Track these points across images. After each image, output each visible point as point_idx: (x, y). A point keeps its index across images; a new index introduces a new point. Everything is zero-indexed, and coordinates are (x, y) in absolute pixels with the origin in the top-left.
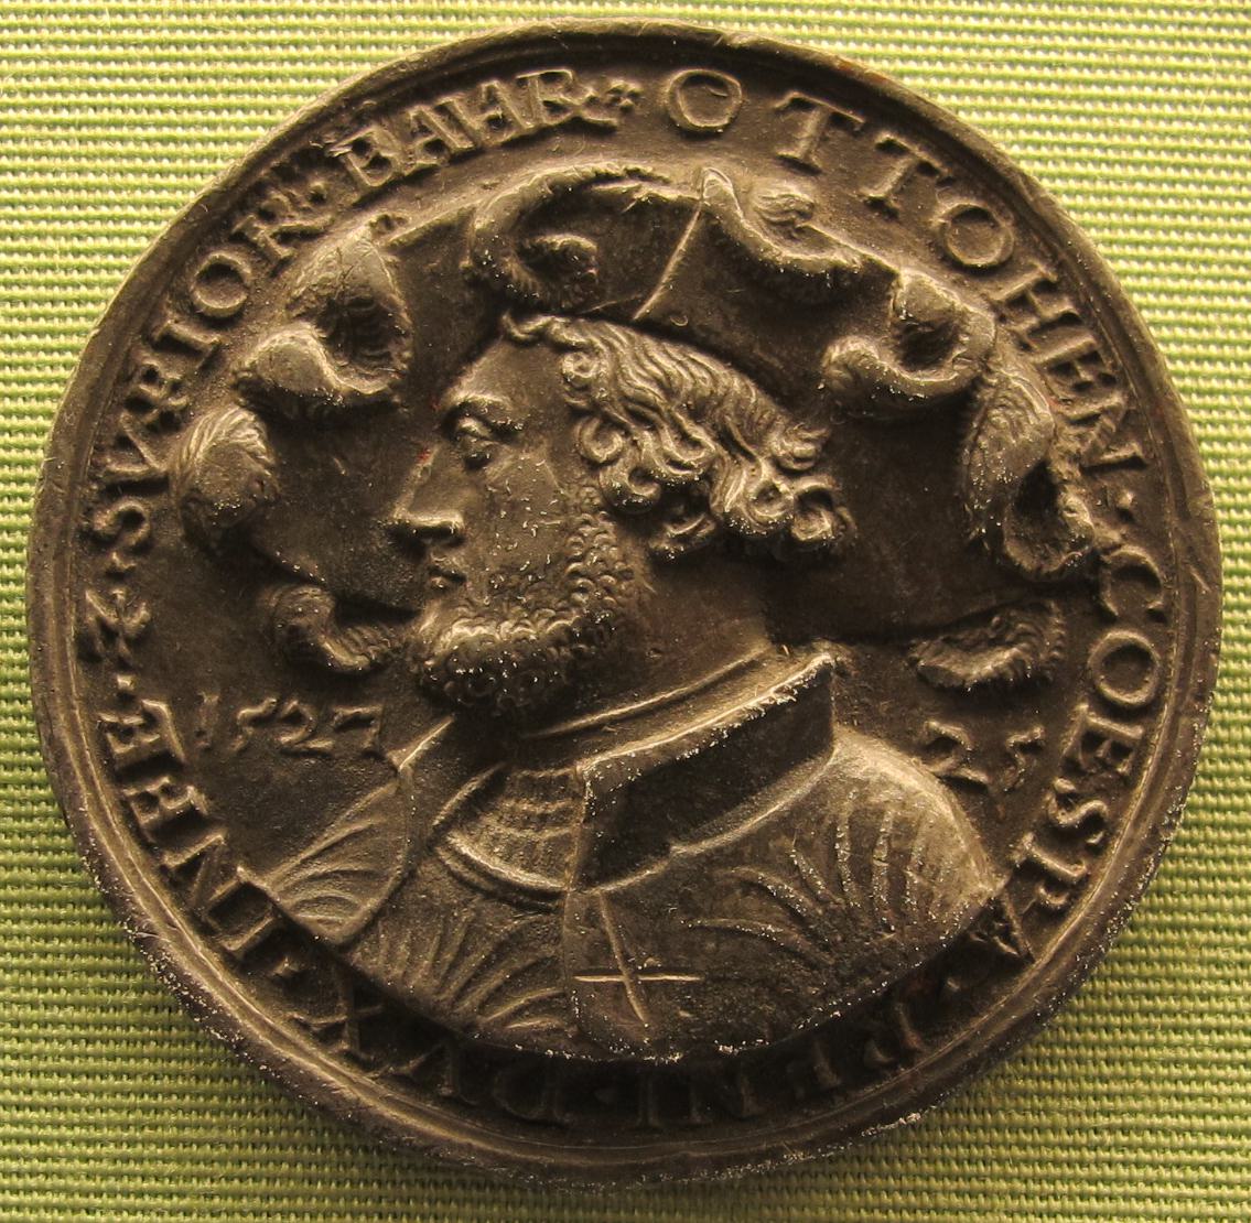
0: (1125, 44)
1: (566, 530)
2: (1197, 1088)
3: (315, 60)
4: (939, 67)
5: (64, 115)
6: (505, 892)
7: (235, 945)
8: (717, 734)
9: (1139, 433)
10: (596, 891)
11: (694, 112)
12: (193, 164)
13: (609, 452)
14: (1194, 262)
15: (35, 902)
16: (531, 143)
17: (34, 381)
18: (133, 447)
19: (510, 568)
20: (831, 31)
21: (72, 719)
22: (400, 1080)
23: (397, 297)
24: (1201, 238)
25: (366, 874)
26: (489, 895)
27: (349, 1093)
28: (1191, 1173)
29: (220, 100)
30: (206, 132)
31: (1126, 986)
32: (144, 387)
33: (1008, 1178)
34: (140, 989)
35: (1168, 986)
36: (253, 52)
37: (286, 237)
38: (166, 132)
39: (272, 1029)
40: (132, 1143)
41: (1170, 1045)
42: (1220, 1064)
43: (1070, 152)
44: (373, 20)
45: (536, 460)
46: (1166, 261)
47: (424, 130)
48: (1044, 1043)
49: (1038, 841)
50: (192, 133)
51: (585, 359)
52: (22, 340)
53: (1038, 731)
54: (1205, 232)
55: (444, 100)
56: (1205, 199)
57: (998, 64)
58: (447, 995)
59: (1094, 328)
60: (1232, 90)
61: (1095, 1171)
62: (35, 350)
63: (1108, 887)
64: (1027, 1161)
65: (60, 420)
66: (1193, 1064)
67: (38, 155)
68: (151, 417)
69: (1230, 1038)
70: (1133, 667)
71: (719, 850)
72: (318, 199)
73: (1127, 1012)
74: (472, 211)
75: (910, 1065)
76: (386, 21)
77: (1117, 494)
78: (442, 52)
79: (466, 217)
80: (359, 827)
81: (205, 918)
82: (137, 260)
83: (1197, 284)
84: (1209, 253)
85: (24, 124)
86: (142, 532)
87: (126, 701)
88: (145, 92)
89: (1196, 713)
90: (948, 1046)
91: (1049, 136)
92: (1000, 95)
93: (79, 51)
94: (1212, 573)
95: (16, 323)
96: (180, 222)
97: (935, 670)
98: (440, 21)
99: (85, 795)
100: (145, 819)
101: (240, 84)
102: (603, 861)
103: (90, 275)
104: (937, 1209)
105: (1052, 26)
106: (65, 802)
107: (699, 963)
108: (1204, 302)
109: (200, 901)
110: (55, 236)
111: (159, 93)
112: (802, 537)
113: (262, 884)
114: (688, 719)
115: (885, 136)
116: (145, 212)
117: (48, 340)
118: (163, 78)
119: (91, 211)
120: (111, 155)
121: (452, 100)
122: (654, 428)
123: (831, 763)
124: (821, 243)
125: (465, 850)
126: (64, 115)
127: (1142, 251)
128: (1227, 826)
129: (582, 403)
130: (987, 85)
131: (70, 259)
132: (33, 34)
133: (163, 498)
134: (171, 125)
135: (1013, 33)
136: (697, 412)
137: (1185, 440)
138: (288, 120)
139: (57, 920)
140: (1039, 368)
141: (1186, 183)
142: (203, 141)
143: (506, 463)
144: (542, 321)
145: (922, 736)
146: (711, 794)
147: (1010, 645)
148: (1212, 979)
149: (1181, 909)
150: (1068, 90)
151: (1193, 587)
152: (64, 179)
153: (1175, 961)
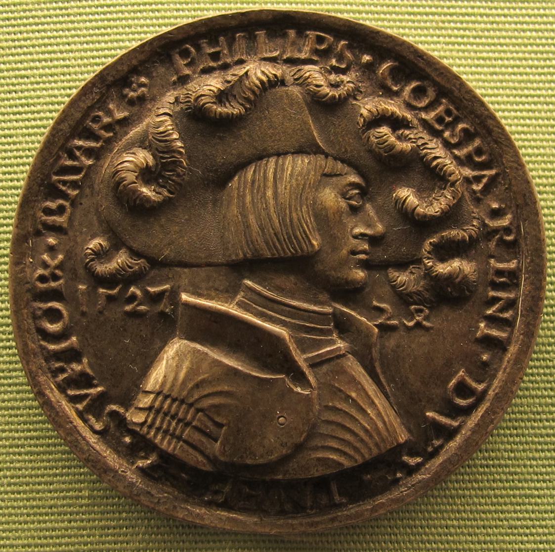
48: (459, 474)
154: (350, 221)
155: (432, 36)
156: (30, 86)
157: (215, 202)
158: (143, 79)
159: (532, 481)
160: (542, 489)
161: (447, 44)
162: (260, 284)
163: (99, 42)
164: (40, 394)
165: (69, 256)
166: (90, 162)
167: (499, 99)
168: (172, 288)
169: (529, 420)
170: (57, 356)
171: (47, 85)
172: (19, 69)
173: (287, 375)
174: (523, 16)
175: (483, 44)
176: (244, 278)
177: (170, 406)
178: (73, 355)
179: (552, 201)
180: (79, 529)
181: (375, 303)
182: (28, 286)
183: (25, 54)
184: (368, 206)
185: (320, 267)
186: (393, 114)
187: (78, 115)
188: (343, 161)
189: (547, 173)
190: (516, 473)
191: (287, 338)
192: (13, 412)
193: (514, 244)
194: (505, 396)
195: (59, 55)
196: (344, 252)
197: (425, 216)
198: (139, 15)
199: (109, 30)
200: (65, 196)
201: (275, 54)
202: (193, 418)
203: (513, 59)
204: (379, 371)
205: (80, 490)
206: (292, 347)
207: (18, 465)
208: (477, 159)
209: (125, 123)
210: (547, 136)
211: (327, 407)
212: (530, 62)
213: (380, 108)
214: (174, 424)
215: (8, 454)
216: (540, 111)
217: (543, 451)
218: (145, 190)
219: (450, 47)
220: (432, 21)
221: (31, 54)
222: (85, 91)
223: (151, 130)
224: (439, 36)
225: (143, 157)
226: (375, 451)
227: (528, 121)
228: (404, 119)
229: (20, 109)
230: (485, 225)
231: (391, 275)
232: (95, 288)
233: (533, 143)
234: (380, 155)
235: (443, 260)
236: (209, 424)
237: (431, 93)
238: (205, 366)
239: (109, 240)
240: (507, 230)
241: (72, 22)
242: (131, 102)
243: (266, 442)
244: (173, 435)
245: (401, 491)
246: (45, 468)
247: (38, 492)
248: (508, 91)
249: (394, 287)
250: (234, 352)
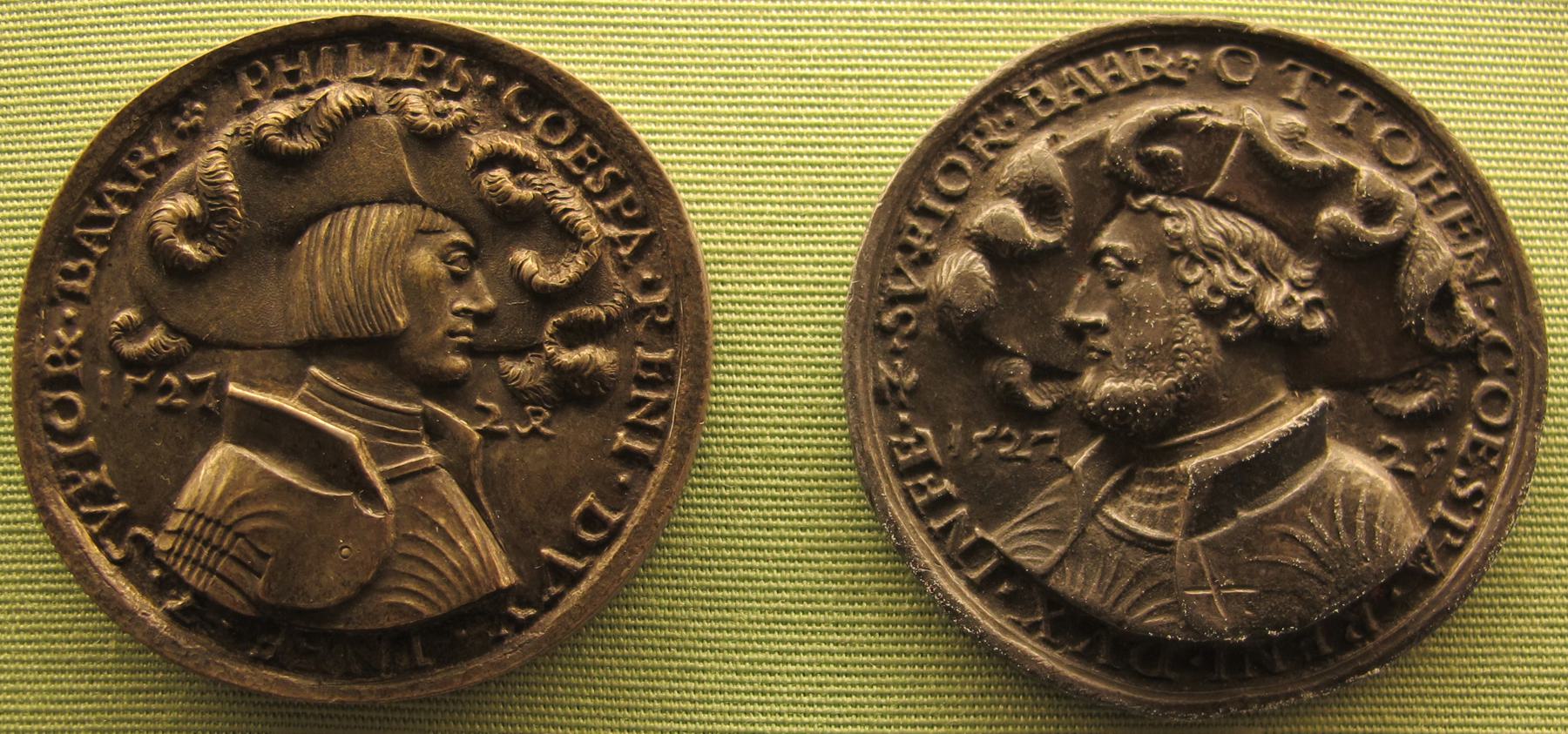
0: (1476, 31)
1: (1172, 324)
2: (1533, 650)
4: (1369, 45)
5: (849, 72)
6: (1139, 541)
7: (975, 575)
8: (1266, 446)
9: (1497, 264)
10: (1195, 540)
11: (1232, 71)
12: (928, 102)
13: (1195, 277)
14: (1520, 161)
15: (846, 550)
16: (1136, 91)
17: (836, 234)
18: (905, 275)
19: (1139, 347)
20: (1305, 23)
21: (874, 440)
22: (1075, 655)
23: (1065, 183)
24: (1523, 147)
25: (1055, 532)
26: (1130, 543)
27: (1047, 663)
28: (1531, 701)
29: (943, 63)
30: (935, 83)
31: (1491, 590)
32: (910, 238)
33: (1426, 705)
34: (911, 602)
35: (1516, 590)
36: (962, 34)
37: (992, 147)
38: (911, 82)
39: (1000, 626)
40: (908, 695)
41: (1518, 625)
42: (1546, 636)
43: (1446, 95)
44: (1033, 15)
45: (1152, 282)
46: (1504, 160)
47: (1072, 83)
49: (1446, 506)
50: (927, 83)
51: (1178, 221)
52: (828, 209)
53: (1444, 441)
54: (1526, 143)
55: (1083, 64)
56: (1525, 123)
57: (1403, 43)
58: (1109, 603)
59: (1469, 201)
60: (1539, 58)
61: (1476, 701)
62: (836, 214)
63: (1488, 533)
64: (1436, 695)
65: (861, 258)
66: (1531, 636)
67: (833, 96)
68: (914, 256)
69: (1552, 620)
70: (1497, 402)
71: (1266, 515)
72: (1009, 124)
73: (1492, 606)
74: (1107, 132)
75: (1372, 639)
76: (1041, 16)
77: (1486, 300)
78: (1082, 35)
79: (1104, 136)
80: (1049, 503)
81: (956, 559)
82: (905, 159)
83: (1522, 174)
84: (1528, 156)
85: (825, 77)
86: (912, 326)
87: (904, 428)
88: (898, 58)
89: (1535, 430)
90: (1394, 629)
91: (1434, 86)
92: (1405, 62)
93: (856, 33)
94: (1542, 345)
95: (823, 198)
96: (928, 138)
97: (1383, 405)
98: (1073, 16)
99: (884, 485)
100: (919, 500)
101: (955, 53)
102: (1199, 523)
103: (868, 169)
104: (1385, 724)
105: (1434, 20)
106: (870, 491)
107: (1256, 582)
108: (1526, 184)
109: (954, 549)
110: (846, 145)
111: (906, 58)
112: (1308, 327)
113: (991, 538)
114: (1245, 436)
115: (1343, 87)
116: (900, 131)
117: (844, 209)
118: (908, 49)
119: (867, 130)
120: (879, 96)
121: (1087, 64)
122: (1221, 263)
123: (1327, 461)
124: (1313, 151)
125: (1115, 516)
126: (849, 72)
127: (1490, 154)
128: (1547, 495)
129: (1176, 247)
130: (1397, 55)
131: (855, 159)
132: (828, 23)
133: (923, 306)
134: (913, 78)
135: (1410, 24)
136: (1245, 253)
137: (1525, 268)
138: (991, 76)
139: (860, 561)
140: (1439, 225)
141: (1513, 114)
142: (934, 88)
143: (1133, 284)
144: (1150, 198)
145: (1376, 444)
146: (1260, 481)
147: (1427, 390)
148: (1540, 585)
149: (1521, 544)
150: (1444, 59)
151: (1532, 355)
152: (850, 111)
153: (1519, 575)
154: (449, 293)
155: (589, 53)
156: (68, 116)
157: (280, 265)
158: (198, 105)
159: (696, 649)
160: (708, 660)
161: (608, 63)
162: (328, 372)
163: (158, 59)
164: (43, 509)
165: (90, 331)
166: (124, 212)
167: (674, 137)
168: (218, 375)
169: (694, 567)
170: (70, 461)
171: (91, 114)
172: (56, 93)
173: (356, 492)
174: (711, 27)
175: (656, 65)
176: (310, 364)
177: (203, 529)
178: (88, 461)
180: (103, 691)
181: (479, 401)
182: (36, 369)
183: (64, 73)
184: (477, 274)
185: (405, 352)
186: (512, 151)
187: (111, 150)
188: (446, 214)
189: (733, 237)
190: (674, 638)
191: (356, 443)
192: (26, 537)
193: (670, 328)
194: (651, 531)
195: (107, 75)
196: (439, 332)
197: (545, 286)
198: (210, 24)
199: (171, 44)
200: (89, 254)
201: (370, 73)
202: (231, 545)
203: (696, 84)
204: (479, 491)
205: (107, 641)
206: (363, 456)
207: (29, 606)
208: (626, 214)
209: (172, 161)
210: (736, 188)
211: (405, 536)
212: (718, 89)
213: (495, 144)
214: (206, 552)
215: (18, 591)
216: (727, 154)
217: (711, 609)
218: (187, 248)
219: (612, 67)
220: (589, 34)
221: (72, 73)
222: (122, 118)
223: (199, 170)
224: (597, 54)
225: (186, 204)
226: (466, 597)
227: (711, 167)
228: (527, 158)
229: (56, 145)
230: (632, 302)
231: (502, 365)
232: (121, 375)
233: (716, 197)
234: (492, 205)
235: (571, 346)
236: (251, 553)
237: (570, 125)
238: (250, 478)
239: (141, 312)
240: (661, 309)
241: (126, 33)
242: (182, 135)
243: (324, 580)
244: (204, 567)
245: (507, 655)
246: (64, 611)
247: (53, 642)
248: (686, 127)
249: (505, 381)
250: (291, 461)
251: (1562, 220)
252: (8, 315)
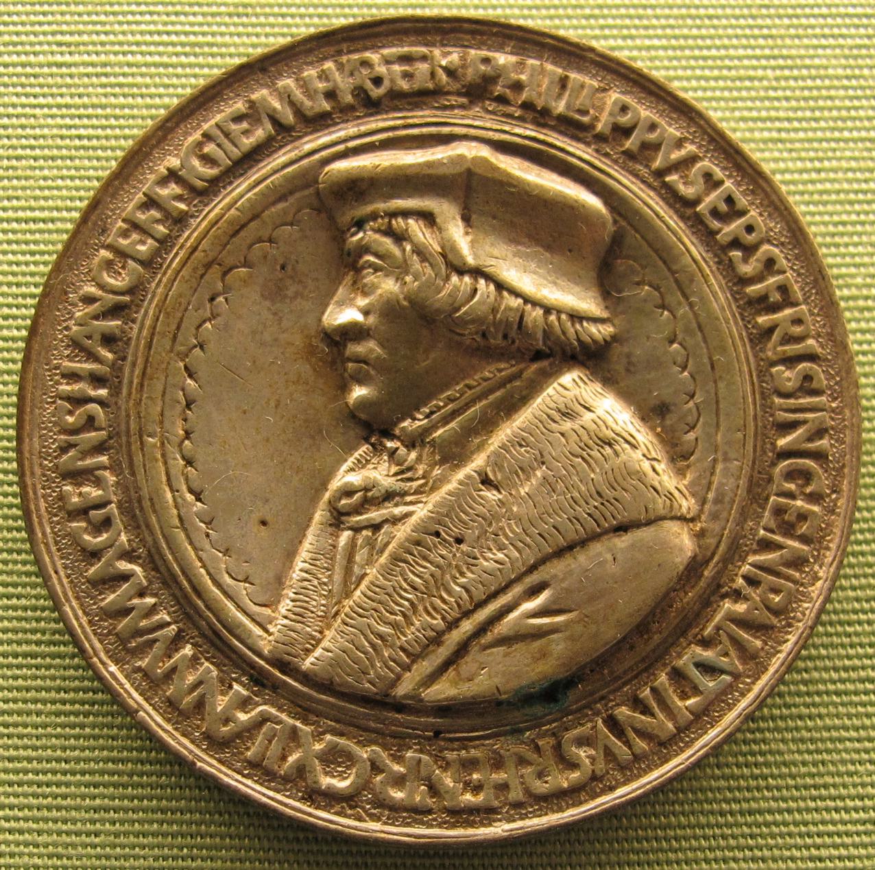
3: (93, 127)
179: (871, 255)
251: (869, 202)
252: (9, 373)
